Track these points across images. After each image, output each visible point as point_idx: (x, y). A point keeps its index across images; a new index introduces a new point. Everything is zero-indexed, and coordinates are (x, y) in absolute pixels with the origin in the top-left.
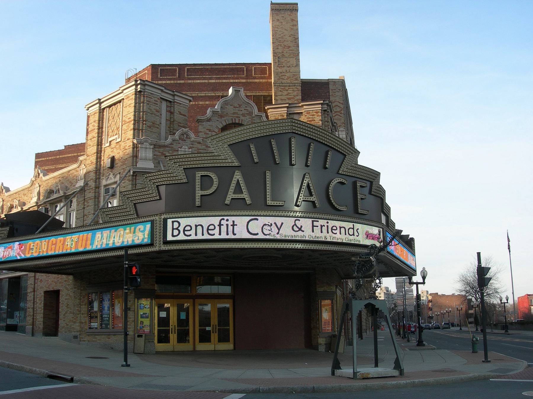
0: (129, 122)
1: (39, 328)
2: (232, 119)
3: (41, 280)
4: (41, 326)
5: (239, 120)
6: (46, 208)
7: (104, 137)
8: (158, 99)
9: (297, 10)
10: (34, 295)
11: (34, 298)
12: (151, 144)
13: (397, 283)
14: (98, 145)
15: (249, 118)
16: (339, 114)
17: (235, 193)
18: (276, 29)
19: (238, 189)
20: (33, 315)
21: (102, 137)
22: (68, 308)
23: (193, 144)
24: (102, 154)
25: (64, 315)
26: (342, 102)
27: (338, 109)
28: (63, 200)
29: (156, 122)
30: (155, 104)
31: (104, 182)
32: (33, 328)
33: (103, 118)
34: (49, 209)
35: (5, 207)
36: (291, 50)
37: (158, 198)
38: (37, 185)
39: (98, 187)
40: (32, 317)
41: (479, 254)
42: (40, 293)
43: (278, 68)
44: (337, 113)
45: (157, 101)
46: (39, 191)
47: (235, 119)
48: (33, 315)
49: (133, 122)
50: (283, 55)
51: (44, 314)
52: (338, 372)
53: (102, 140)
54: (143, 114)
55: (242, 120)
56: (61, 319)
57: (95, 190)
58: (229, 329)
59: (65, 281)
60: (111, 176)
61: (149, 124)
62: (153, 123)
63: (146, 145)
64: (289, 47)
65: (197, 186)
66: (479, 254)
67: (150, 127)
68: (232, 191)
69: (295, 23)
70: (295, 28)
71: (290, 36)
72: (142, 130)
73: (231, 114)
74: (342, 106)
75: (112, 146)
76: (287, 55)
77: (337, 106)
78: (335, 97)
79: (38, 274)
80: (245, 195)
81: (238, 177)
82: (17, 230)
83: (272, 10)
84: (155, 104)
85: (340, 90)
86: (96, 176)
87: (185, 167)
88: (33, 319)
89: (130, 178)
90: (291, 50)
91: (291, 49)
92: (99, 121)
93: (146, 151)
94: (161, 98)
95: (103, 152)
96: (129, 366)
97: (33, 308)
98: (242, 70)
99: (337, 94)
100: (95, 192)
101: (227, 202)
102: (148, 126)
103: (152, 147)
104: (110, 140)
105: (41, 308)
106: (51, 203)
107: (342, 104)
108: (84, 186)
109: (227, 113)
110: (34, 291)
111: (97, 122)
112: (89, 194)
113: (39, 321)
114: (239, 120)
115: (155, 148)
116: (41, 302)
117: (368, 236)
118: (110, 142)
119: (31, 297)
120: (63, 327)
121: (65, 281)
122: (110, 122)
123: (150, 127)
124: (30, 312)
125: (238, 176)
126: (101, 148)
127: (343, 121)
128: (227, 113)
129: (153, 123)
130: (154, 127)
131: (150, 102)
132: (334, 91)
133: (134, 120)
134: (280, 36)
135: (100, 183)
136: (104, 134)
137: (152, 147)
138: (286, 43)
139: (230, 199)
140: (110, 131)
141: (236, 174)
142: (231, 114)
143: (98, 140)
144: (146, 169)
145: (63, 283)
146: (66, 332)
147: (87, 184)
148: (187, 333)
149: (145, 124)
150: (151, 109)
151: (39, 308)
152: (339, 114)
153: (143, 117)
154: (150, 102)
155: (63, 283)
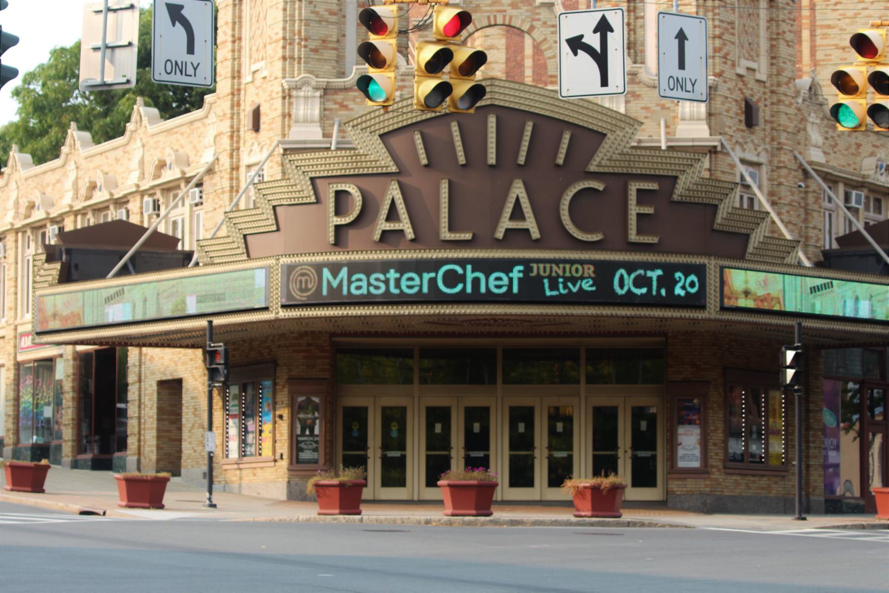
0: (277, 41)
1: (151, 460)
2: (489, 18)
3: (152, 357)
4: (154, 457)
5: (504, 17)
6: (154, 201)
7: (243, 59)
10: (140, 389)
11: (140, 396)
12: (316, 89)
14: (233, 78)
15: (527, 11)
17: (512, 218)
19: (517, 213)
20: (139, 433)
21: (240, 58)
22: (195, 415)
23: (403, 80)
24: (242, 96)
25: (190, 431)
28: (183, 185)
29: (331, 36)
31: (246, 160)
32: (139, 461)
33: (240, 17)
34: (161, 201)
35: (81, 183)
37: (274, 228)
38: (138, 144)
39: (235, 168)
40: (136, 438)
42: (151, 386)
46: (143, 159)
47: (495, 17)
48: (139, 433)
49: (281, 43)
51: (159, 430)
53: (240, 65)
54: (300, 26)
55: (511, 18)
56: (185, 440)
57: (231, 173)
58: (345, 449)
59: (191, 360)
60: (256, 147)
61: (313, 44)
62: (324, 41)
63: (307, 91)
67: (315, 51)
72: (300, 58)
73: (487, 5)
75: (258, 82)
79: (144, 349)
80: (530, 224)
82: (76, 266)
86: (232, 145)
87: (382, 132)
88: (139, 441)
89: (279, 159)
92: (234, 23)
93: (306, 104)
95: (242, 92)
96: (213, 506)
97: (139, 418)
100: (231, 179)
101: (500, 235)
102: (312, 50)
103: (318, 94)
104: (254, 68)
105: (152, 417)
106: (163, 190)
108: (213, 163)
109: (478, 6)
110: (140, 381)
111: (230, 25)
112: (221, 181)
113: (149, 446)
114: (504, 17)
115: (325, 94)
116: (152, 405)
118: (254, 72)
119: (134, 393)
120: (189, 457)
121: (191, 360)
122: (254, 29)
123: (315, 51)
124: (133, 427)
126: (239, 84)
128: (478, 6)
129: (324, 41)
130: (325, 48)
133: (284, 38)
135: (239, 160)
136: (243, 53)
137: (318, 94)
140: (254, 48)
142: (487, 5)
143: (233, 65)
144: (305, 142)
145: (186, 363)
146: (192, 466)
147: (218, 159)
148: (401, 463)
149: (305, 46)
150: (317, 13)
151: (150, 417)
153: (300, 32)
155: (186, 363)
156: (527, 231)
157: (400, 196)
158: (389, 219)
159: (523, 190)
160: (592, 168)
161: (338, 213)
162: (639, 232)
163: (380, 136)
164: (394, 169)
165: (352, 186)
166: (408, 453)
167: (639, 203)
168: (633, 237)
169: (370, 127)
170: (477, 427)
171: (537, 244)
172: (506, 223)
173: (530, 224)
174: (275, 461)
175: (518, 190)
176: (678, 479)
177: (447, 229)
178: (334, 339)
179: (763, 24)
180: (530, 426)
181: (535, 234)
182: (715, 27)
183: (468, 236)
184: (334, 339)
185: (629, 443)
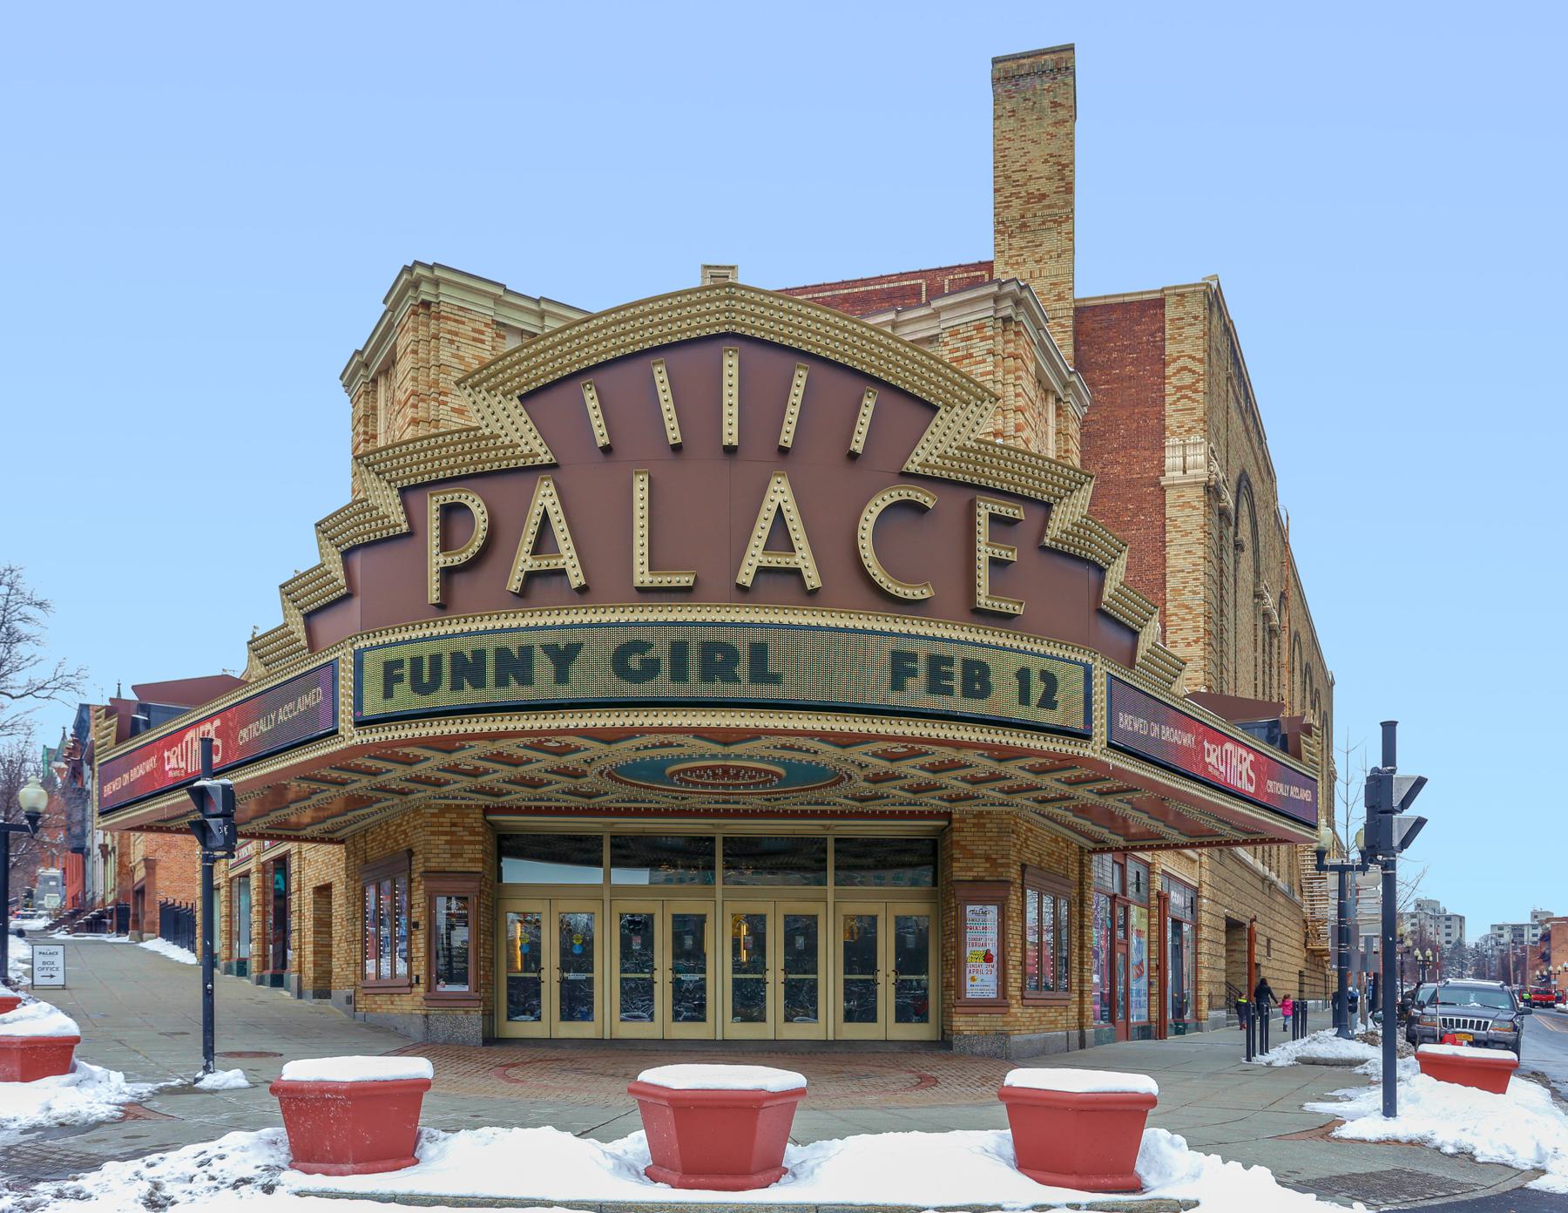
8: (486, 325)
9: (1070, 70)
13: (1067, 252)
16: (1190, 393)
18: (1006, 144)
19: (780, 537)
26: (1200, 355)
27: (1188, 379)
30: (474, 339)
36: (1049, 207)
41: (1389, 728)
43: (1008, 269)
44: (1184, 392)
45: (482, 333)
50: (1024, 225)
52: (1259, 1059)
64: (1044, 196)
65: (637, 560)
66: (1389, 728)
68: (762, 543)
69: (1062, 113)
70: (1062, 131)
71: (1046, 161)
74: (1199, 368)
76: (1034, 224)
77: (1184, 368)
78: (1182, 342)
81: (779, 498)
83: (996, 81)
84: (474, 339)
85: (1196, 318)
90: (1049, 207)
91: (1046, 202)
94: (498, 323)
98: (916, 291)
99: (1188, 331)
101: (746, 577)
107: (1201, 361)
117: (1369, 940)
125: (545, 497)
127: (1199, 413)
131: (456, 334)
132: (1180, 323)
134: (1016, 167)
138: (1032, 187)
139: (752, 571)
141: (773, 486)
148: (647, 988)
150: (462, 359)
152: (1190, 393)
154: (456, 334)
156: (797, 572)
157: (558, 507)
158: (536, 550)
159: (789, 496)
160: (912, 468)
161: (445, 546)
162: (994, 592)
163: (521, 398)
164: (546, 459)
165: (478, 501)
166: (597, 975)
167: (993, 539)
168: (983, 601)
169: (503, 384)
170: (800, 942)
171: (811, 597)
172: (756, 556)
173: (803, 558)
174: (411, 986)
175: (780, 494)
176: (967, 1014)
177: (646, 568)
178: (490, 818)
179: (1051, 432)
180: (648, 944)
181: (813, 580)
182: (1017, 395)
183: (685, 580)
184: (490, 818)
185: (892, 965)
